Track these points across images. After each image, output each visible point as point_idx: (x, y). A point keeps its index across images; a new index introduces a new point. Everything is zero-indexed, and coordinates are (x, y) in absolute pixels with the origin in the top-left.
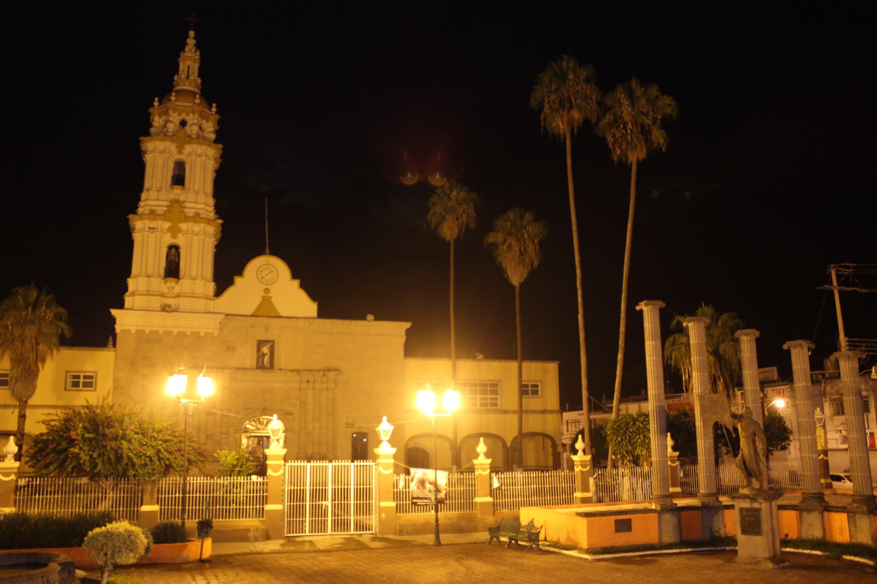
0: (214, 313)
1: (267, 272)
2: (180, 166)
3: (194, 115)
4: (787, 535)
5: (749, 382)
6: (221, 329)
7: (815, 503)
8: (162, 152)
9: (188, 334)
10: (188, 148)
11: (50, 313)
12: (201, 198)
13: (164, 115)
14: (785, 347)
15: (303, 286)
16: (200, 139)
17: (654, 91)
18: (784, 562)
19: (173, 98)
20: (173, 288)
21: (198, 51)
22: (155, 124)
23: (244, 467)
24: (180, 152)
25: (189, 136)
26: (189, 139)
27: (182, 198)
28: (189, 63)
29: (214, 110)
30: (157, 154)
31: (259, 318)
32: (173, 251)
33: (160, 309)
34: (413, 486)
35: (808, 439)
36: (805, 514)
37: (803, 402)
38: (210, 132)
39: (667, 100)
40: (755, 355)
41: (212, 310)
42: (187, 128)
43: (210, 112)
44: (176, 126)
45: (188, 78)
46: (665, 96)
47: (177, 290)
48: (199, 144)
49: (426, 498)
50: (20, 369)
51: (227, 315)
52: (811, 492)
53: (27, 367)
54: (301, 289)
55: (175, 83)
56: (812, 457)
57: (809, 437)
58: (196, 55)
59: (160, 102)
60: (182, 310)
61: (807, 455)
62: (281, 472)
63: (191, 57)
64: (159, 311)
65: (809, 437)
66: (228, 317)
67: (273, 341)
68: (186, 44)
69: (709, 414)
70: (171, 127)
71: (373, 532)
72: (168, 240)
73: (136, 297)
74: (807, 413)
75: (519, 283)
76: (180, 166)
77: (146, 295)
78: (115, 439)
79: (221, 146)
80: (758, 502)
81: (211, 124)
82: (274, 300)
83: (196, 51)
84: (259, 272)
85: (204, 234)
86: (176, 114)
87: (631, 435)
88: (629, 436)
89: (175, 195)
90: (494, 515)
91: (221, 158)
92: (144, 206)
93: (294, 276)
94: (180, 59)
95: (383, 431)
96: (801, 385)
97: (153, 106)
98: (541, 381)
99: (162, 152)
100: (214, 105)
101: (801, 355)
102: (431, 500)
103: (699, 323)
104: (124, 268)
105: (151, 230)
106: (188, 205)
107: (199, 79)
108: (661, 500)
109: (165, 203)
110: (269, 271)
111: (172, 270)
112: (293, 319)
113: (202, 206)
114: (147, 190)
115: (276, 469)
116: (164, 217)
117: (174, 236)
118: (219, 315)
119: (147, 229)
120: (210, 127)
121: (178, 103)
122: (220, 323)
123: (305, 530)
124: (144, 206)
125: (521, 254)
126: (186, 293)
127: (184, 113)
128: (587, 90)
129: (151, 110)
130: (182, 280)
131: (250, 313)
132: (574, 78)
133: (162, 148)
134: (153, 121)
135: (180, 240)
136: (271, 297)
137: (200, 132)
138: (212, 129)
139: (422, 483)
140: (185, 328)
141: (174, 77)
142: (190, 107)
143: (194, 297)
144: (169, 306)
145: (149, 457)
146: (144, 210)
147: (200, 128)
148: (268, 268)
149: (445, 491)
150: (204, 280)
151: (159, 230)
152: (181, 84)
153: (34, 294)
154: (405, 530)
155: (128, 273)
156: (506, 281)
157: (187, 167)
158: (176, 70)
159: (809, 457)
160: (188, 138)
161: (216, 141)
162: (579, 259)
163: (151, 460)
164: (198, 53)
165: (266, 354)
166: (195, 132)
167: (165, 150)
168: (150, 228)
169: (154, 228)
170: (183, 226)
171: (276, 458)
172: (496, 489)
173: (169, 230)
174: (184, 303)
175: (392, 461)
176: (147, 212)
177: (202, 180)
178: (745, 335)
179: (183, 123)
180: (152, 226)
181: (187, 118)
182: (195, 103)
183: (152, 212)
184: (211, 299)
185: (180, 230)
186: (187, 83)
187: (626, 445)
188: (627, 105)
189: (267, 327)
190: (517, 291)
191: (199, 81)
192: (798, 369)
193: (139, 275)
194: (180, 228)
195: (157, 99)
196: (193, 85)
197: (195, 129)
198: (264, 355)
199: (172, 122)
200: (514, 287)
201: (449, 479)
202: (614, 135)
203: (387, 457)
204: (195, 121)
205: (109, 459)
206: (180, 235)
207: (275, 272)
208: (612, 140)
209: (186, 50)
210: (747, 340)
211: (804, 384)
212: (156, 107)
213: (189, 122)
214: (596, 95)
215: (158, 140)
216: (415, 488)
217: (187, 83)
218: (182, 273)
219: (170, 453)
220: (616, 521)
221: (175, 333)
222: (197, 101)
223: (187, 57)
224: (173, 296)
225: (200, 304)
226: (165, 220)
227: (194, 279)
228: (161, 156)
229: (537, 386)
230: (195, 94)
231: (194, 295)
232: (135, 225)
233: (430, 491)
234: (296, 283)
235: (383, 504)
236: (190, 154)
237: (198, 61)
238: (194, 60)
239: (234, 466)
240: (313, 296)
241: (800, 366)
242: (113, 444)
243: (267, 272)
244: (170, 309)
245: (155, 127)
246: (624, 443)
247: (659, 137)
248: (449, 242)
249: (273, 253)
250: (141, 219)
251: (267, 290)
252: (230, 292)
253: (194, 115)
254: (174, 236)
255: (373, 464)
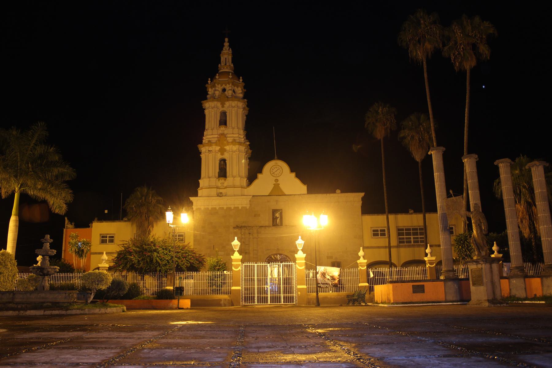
0: (246, 195)
1: (276, 169)
2: (224, 115)
3: (229, 85)
4: (535, 295)
5: (505, 194)
6: (250, 204)
7: (550, 271)
8: (212, 108)
9: (233, 208)
10: (227, 104)
11: (154, 200)
12: (236, 130)
13: (213, 87)
14: (495, 163)
15: (297, 176)
16: (234, 97)
17: (477, 19)
18: (502, 303)
19: (217, 77)
20: (223, 183)
21: (230, 49)
22: (209, 93)
23: (221, 267)
24: (223, 107)
25: (227, 97)
26: (228, 99)
27: (226, 132)
28: (226, 56)
29: (241, 80)
30: (210, 109)
31: (272, 196)
32: (222, 162)
33: (216, 196)
34: (319, 276)
35: (544, 228)
36: (544, 279)
37: (540, 203)
38: (240, 93)
39: (487, 24)
40: (475, 170)
41: (246, 195)
42: (226, 93)
43: (239, 82)
44: (220, 92)
45: (226, 64)
46: (485, 22)
47: (225, 185)
48: (232, 100)
49: (327, 284)
50: (140, 231)
51: (253, 196)
52: (549, 264)
53: (144, 230)
54: (296, 178)
55: (219, 69)
56: (548, 240)
57: (545, 226)
58: (229, 51)
59: (211, 81)
60: (228, 195)
61: (545, 239)
62: (240, 268)
63: (227, 52)
64: (216, 197)
65: (545, 226)
66: (254, 197)
67: (282, 210)
68: (224, 46)
69: (452, 210)
70: (217, 93)
71: (295, 303)
72: (219, 156)
73: (203, 189)
74: (543, 210)
75: (421, 160)
76: (224, 115)
77: (209, 188)
78: (151, 251)
79: (246, 100)
80: (480, 264)
81: (240, 89)
82: (281, 186)
83: (229, 49)
84: (271, 170)
85: (239, 151)
86: (219, 86)
87: (468, 244)
88: (467, 245)
89: (222, 131)
90: (370, 294)
91: (247, 106)
92: (205, 139)
93: (292, 171)
94: (221, 55)
95: (298, 244)
96: (538, 191)
97: (208, 83)
98: (455, 225)
99: (212, 108)
100: (241, 78)
101: (537, 171)
102: (329, 285)
103: (470, 158)
104: (198, 175)
105: (209, 152)
106: (228, 135)
107: (232, 64)
108: (446, 273)
109: (216, 136)
110: (277, 169)
111: (223, 173)
112: (292, 196)
113: (237, 135)
114: (207, 130)
115: (237, 267)
116: (216, 144)
117: (222, 154)
118: (250, 196)
119: (207, 152)
120: (240, 90)
121: (219, 79)
122: (250, 201)
123: (255, 302)
124: (205, 139)
125: (420, 141)
126: (230, 185)
127: (224, 85)
128: (434, 28)
129: (207, 85)
130: (228, 178)
131: (267, 194)
132: (424, 22)
133: (213, 105)
134: (208, 91)
135: (226, 156)
136: (279, 184)
137: (234, 94)
138: (240, 91)
139: (324, 275)
140: (223, 205)
141: (218, 65)
142: (227, 80)
143: (235, 187)
144: (221, 193)
145: (167, 260)
146: (205, 141)
147: (234, 91)
148: (276, 168)
149: (338, 279)
150: (240, 177)
151: (214, 151)
152: (222, 68)
153: (146, 190)
154: (312, 302)
155: (199, 177)
156: (413, 159)
157: (227, 114)
158: (219, 61)
159: (546, 240)
160: (226, 98)
161: (244, 98)
162: (435, 136)
163: (169, 262)
164: (230, 50)
165: (278, 217)
166: (230, 94)
167: (214, 106)
168: (209, 151)
169: (211, 151)
170: (227, 148)
171: (236, 260)
172: (372, 278)
173: (220, 151)
174: (230, 191)
175: (304, 261)
176: (207, 142)
177: (236, 122)
178: (501, 163)
179: (224, 90)
180: (210, 149)
181: (225, 87)
182: (229, 78)
183: (209, 141)
184: (245, 188)
185: (225, 150)
186: (225, 68)
187: (465, 251)
188: (460, 33)
189: (277, 201)
190: (420, 165)
191: (232, 65)
192: (535, 181)
193: (205, 177)
194: (225, 149)
195: (209, 79)
196: (229, 68)
197: (230, 92)
198: (277, 218)
199: (218, 90)
200: (418, 162)
201: (341, 272)
202: (454, 54)
203: (301, 259)
204: (230, 88)
205: (147, 261)
206: (225, 153)
207: (281, 169)
208: (453, 57)
209: (224, 49)
210: (503, 166)
211: (540, 190)
212: (209, 84)
213: (227, 89)
214: (439, 31)
215: (210, 101)
216: (320, 277)
217: (225, 68)
218: (228, 174)
219: (179, 258)
220: (413, 285)
221: (225, 208)
222: (230, 77)
223: (224, 53)
224: (223, 187)
225: (238, 191)
226: (216, 145)
227: (235, 177)
228: (213, 110)
229: (452, 228)
230: (229, 72)
231: (235, 186)
232: (201, 150)
233: (328, 279)
234: (293, 175)
235: (299, 287)
236: (229, 107)
237: (231, 54)
238: (229, 54)
239: (216, 266)
240: (304, 181)
241: (537, 179)
242: (149, 254)
243: (276, 169)
244: (221, 195)
245: (210, 95)
246: (464, 250)
247: (484, 50)
248: (380, 140)
249: (280, 158)
250: (203, 146)
251: (277, 180)
252: (256, 183)
253: (229, 85)
254: (222, 154)
255: (294, 264)
